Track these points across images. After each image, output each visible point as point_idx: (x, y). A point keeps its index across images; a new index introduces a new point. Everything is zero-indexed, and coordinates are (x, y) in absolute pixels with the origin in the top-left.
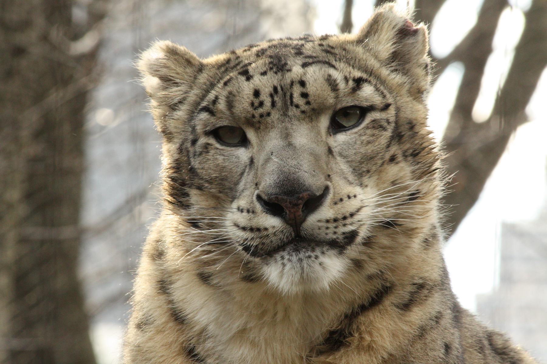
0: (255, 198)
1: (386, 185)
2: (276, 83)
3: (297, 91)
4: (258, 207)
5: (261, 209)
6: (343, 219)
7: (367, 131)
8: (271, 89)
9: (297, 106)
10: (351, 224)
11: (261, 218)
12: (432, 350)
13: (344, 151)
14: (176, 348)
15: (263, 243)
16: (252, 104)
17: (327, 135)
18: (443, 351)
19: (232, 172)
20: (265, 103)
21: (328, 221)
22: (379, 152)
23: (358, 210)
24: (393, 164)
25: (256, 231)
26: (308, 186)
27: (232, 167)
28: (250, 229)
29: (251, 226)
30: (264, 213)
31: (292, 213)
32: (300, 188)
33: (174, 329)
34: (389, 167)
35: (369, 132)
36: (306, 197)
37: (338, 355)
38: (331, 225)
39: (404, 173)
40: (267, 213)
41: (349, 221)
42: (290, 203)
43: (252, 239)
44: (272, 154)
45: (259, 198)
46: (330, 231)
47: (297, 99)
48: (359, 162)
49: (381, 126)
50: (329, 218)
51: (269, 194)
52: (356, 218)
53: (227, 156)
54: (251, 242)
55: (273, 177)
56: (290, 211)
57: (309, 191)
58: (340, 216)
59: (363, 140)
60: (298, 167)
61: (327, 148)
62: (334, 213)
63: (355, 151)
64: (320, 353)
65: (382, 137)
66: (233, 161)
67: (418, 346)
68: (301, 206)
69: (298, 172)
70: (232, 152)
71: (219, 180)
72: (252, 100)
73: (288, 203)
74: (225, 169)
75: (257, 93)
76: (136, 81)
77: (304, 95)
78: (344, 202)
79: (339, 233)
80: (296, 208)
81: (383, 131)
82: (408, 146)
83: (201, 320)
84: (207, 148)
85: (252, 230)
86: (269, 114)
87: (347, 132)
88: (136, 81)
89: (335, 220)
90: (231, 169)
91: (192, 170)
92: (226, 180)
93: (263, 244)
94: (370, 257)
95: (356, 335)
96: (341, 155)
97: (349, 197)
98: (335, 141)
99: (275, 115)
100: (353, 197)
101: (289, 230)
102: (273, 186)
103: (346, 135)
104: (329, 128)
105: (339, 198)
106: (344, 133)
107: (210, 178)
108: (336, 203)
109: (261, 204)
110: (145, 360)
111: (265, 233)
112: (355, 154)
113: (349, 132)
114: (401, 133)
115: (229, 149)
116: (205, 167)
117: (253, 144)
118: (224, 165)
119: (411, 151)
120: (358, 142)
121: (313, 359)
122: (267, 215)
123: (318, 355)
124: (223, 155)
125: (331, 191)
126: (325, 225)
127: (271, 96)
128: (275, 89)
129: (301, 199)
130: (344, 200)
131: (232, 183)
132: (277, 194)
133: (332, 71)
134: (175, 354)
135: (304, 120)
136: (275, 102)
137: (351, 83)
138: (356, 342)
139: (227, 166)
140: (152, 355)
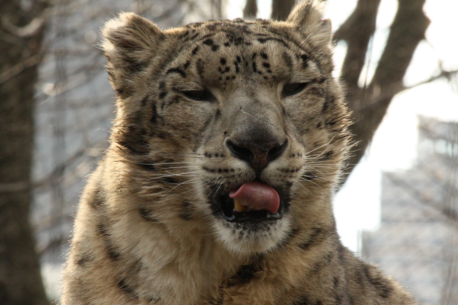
0: (224, 143)
2: (239, 53)
3: (259, 62)
4: (228, 151)
5: (230, 153)
7: (308, 96)
8: (235, 59)
9: (260, 73)
11: (230, 160)
12: (325, 283)
14: (110, 280)
15: (229, 182)
16: (220, 69)
18: (332, 284)
19: (199, 120)
22: (317, 114)
25: (224, 172)
27: (198, 116)
28: (218, 171)
29: (220, 168)
30: (232, 157)
31: (259, 158)
32: (269, 138)
37: (248, 287)
40: (235, 157)
42: (259, 149)
43: (220, 178)
44: (241, 108)
45: (229, 143)
47: (260, 67)
48: (302, 121)
51: (241, 140)
53: (194, 107)
54: (218, 182)
55: (244, 127)
56: (257, 156)
59: (306, 103)
60: (266, 119)
63: (299, 111)
64: (230, 285)
65: (320, 102)
66: (199, 111)
67: (314, 279)
68: (267, 153)
70: (198, 105)
71: (185, 126)
72: (219, 66)
74: (192, 117)
76: (98, 46)
77: (266, 65)
81: (320, 97)
82: (329, 116)
83: (121, 253)
84: (177, 99)
85: (220, 171)
86: (234, 77)
88: (98, 46)
90: (197, 118)
91: (154, 118)
92: (192, 126)
93: (229, 183)
95: (266, 269)
98: (285, 103)
99: (239, 79)
101: (253, 173)
102: (245, 134)
103: (292, 99)
107: (177, 124)
108: (290, 157)
109: (230, 149)
110: (84, 291)
111: (232, 174)
112: (299, 114)
113: (294, 96)
115: (195, 101)
116: (174, 114)
117: (219, 100)
118: (191, 114)
119: (330, 120)
120: (302, 104)
121: (224, 289)
122: (235, 158)
123: (229, 286)
124: (191, 106)
127: (236, 63)
128: (238, 58)
131: (198, 129)
132: (249, 141)
134: (110, 285)
136: (239, 68)
138: (265, 276)
139: (194, 115)
140: (89, 287)
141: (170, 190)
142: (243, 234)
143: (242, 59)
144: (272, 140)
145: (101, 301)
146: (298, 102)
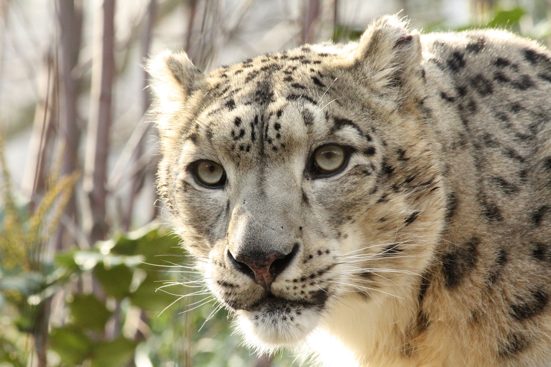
6: (310, 277)
9: (270, 141)
16: (233, 133)
17: (303, 180)
20: (246, 131)
21: (295, 281)
23: (329, 268)
36: (272, 258)
38: (299, 285)
42: (256, 264)
47: (272, 133)
61: (301, 195)
62: (302, 272)
68: (269, 267)
73: (254, 264)
75: (238, 121)
77: (277, 126)
79: (307, 293)
80: (263, 269)
87: (328, 179)
89: (303, 279)
97: (320, 253)
100: (325, 253)
103: (326, 182)
104: (304, 171)
106: (324, 180)
125: (302, 249)
126: (292, 285)
127: (252, 125)
128: (256, 118)
129: (268, 260)
133: (309, 106)
137: (331, 122)
143: (259, 120)
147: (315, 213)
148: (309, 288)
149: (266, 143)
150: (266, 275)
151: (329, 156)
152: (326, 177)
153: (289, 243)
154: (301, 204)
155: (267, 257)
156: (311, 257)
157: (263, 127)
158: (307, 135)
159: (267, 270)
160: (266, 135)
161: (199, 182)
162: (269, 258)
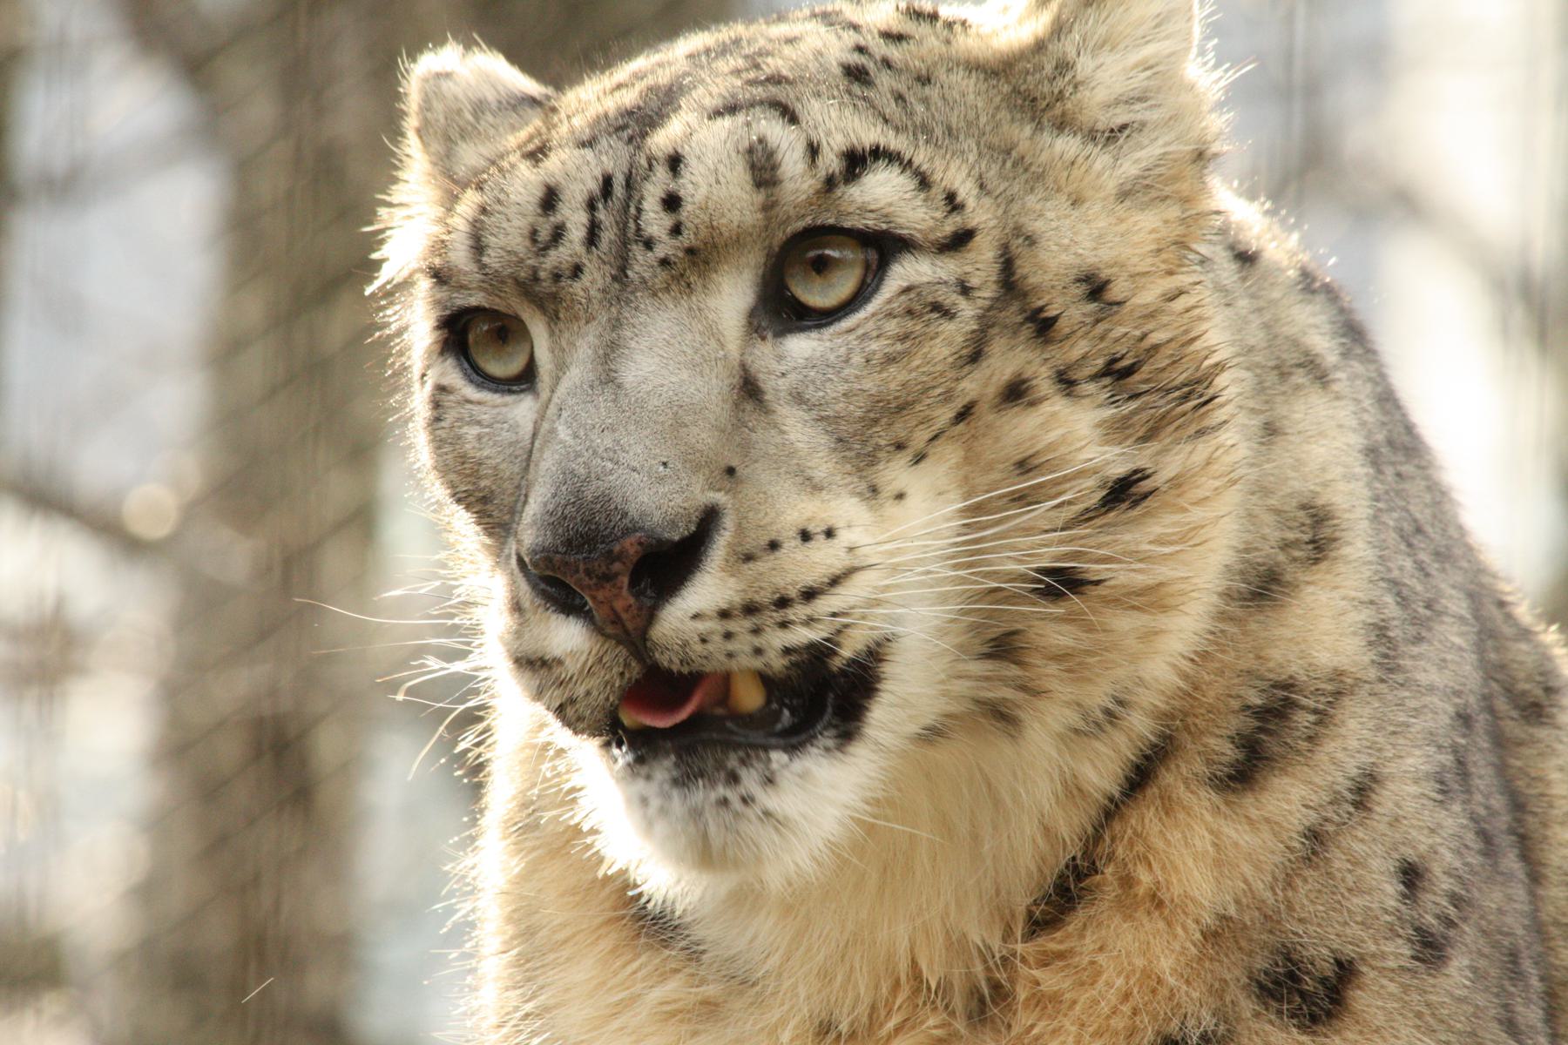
1: (995, 476)
6: (775, 605)
8: (594, 186)
9: (649, 244)
10: (810, 621)
13: (811, 388)
16: (533, 234)
21: (724, 614)
23: (835, 581)
24: (1016, 409)
26: (637, 518)
33: (648, 902)
34: (1004, 419)
35: (892, 327)
36: (632, 551)
38: (740, 626)
39: (1060, 432)
41: (799, 611)
42: (588, 573)
46: (743, 644)
47: (655, 222)
48: (862, 419)
49: (936, 307)
50: (725, 606)
52: (824, 605)
57: (642, 529)
58: (765, 597)
59: (874, 353)
62: (742, 586)
68: (625, 580)
69: (611, 472)
70: (504, 410)
73: (582, 575)
75: (550, 199)
77: (672, 202)
78: (783, 551)
80: (608, 586)
86: (577, 271)
87: (824, 331)
89: (750, 609)
94: (1023, 688)
96: (798, 398)
97: (805, 536)
98: (780, 358)
104: (752, 314)
105: (764, 540)
106: (814, 334)
108: (749, 558)
114: (1041, 309)
120: (857, 359)
125: (728, 522)
127: (591, 206)
128: (607, 182)
129: (619, 557)
130: (785, 545)
135: (667, 289)
141: (882, 533)
142: (1247, 323)
143: (618, 190)
144: (627, 532)
145: (898, 587)
146: (843, 350)
147: (784, 428)
148: (777, 640)
149: (637, 250)
150: (624, 600)
151: (822, 266)
152: (819, 327)
153: (685, 505)
154: (736, 405)
155: (617, 548)
156: (774, 546)
157: (626, 207)
158: (760, 216)
159: (621, 588)
160: (639, 229)
161: (474, 376)
162: (621, 552)
